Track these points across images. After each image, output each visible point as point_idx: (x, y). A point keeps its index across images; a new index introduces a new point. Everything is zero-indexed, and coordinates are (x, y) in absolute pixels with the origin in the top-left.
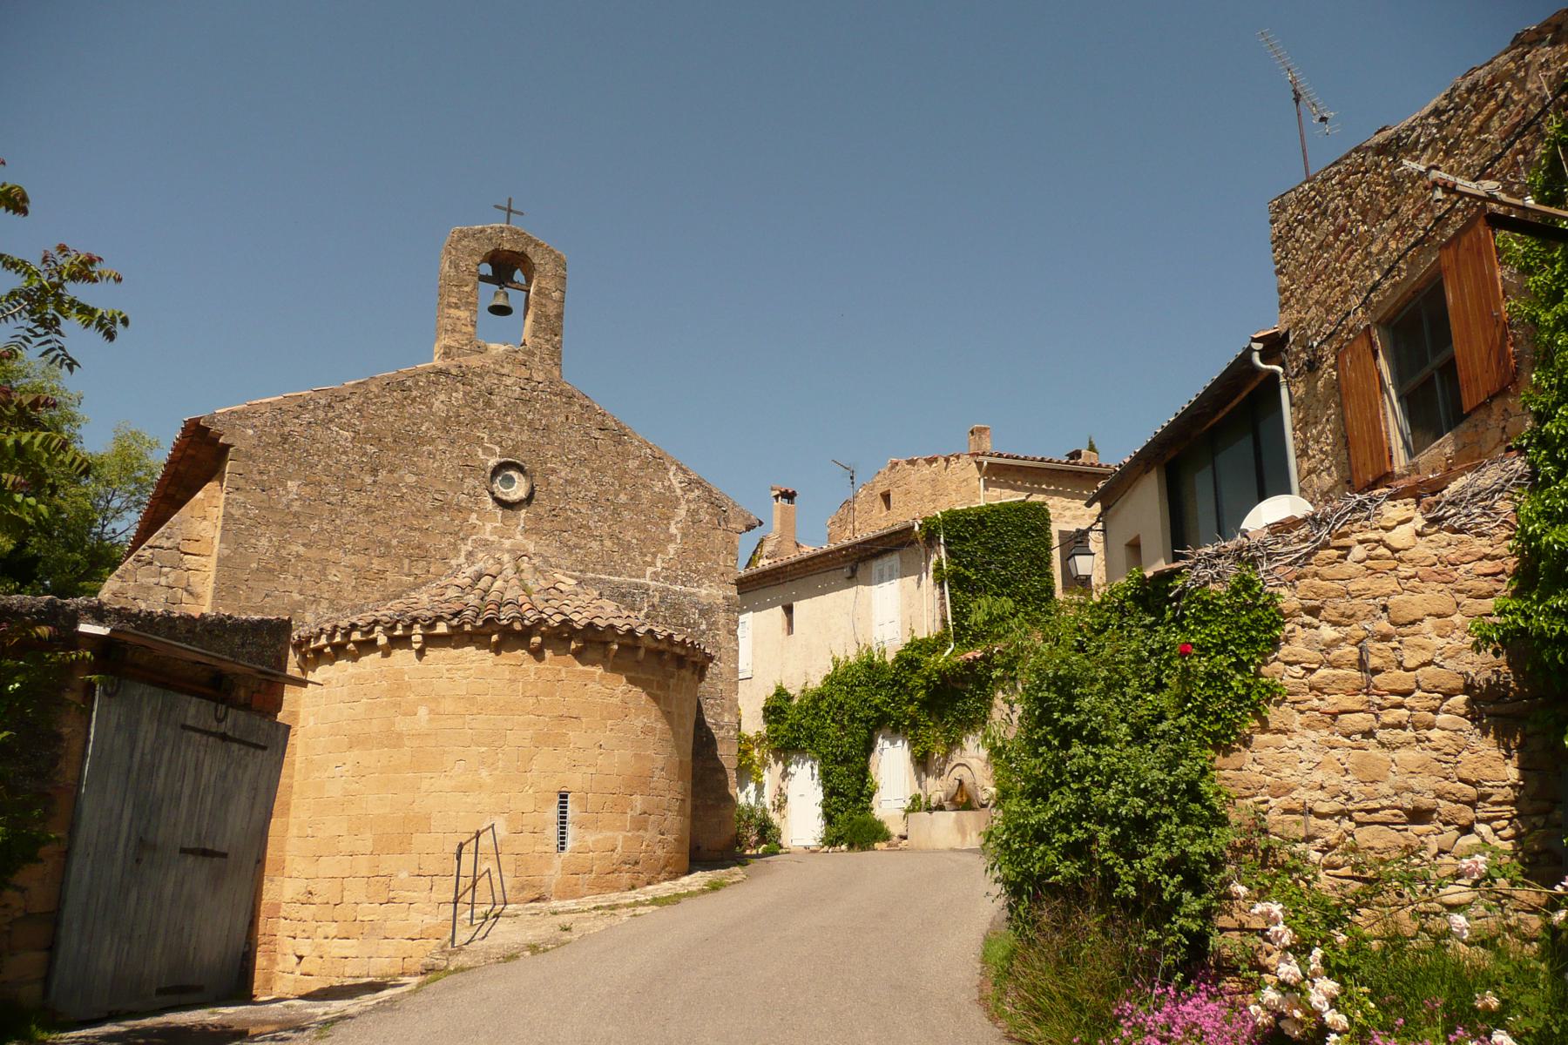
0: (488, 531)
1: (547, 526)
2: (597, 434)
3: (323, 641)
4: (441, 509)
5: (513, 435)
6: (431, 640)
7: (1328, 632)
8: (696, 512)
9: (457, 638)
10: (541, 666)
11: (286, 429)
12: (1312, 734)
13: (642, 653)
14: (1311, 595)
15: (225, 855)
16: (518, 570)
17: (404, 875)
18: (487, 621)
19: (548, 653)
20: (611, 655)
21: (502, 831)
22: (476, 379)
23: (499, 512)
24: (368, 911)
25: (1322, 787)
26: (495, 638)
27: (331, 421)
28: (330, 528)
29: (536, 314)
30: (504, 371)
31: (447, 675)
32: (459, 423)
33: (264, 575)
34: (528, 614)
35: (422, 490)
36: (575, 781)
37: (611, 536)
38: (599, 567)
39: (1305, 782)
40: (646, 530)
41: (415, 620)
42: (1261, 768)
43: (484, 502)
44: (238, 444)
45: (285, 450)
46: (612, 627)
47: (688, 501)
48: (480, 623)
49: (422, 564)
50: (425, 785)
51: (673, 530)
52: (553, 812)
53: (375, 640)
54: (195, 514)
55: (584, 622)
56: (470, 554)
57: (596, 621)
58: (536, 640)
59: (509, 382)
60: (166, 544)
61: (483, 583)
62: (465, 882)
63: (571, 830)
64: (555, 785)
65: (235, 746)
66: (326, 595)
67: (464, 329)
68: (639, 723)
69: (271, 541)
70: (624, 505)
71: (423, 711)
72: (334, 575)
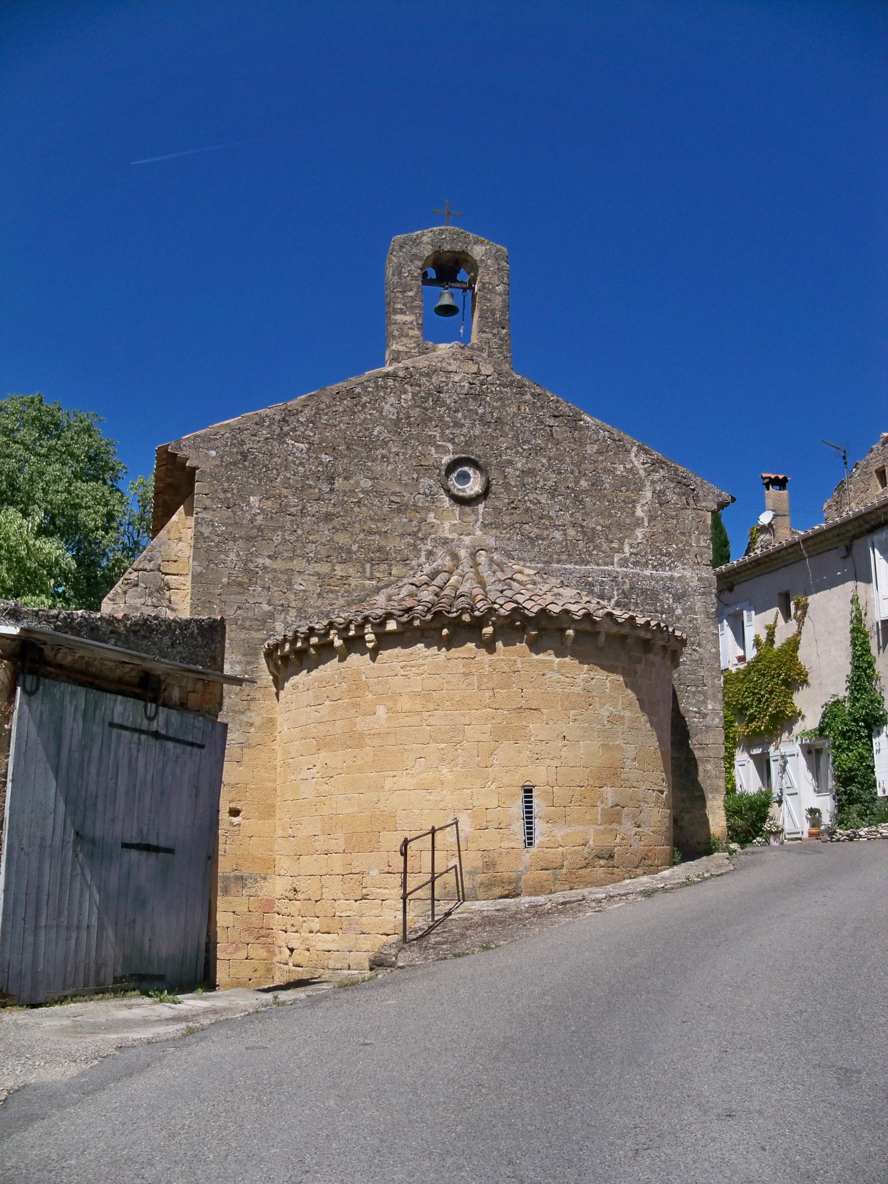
0: (446, 530)
1: (507, 520)
2: (551, 422)
3: (287, 647)
4: (399, 511)
5: (465, 430)
6: (386, 641)
8: (662, 493)
9: (407, 636)
10: (493, 657)
11: (245, 447)
13: (602, 638)
15: (170, 851)
16: (475, 565)
17: (374, 873)
18: (438, 614)
19: (499, 644)
20: (569, 643)
21: (466, 826)
22: (424, 380)
23: (457, 509)
24: (347, 908)
26: (445, 632)
27: (287, 435)
28: (293, 538)
29: (481, 310)
30: (450, 368)
32: (409, 424)
33: (236, 589)
34: (479, 605)
35: (380, 494)
36: (539, 775)
37: (574, 525)
38: (564, 557)
40: (610, 515)
43: (439, 500)
44: (203, 467)
45: (245, 468)
46: (567, 612)
48: (429, 617)
50: (389, 783)
51: (639, 513)
52: (517, 807)
53: (332, 642)
54: (172, 536)
55: (535, 610)
56: (430, 553)
58: (488, 630)
59: (457, 378)
60: (149, 566)
61: (439, 581)
63: (539, 825)
65: (170, 745)
67: (411, 333)
68: (604, 712)
69: (238, 555)
70: (585, 491)
71: (381, 710)
72: (300, 584)
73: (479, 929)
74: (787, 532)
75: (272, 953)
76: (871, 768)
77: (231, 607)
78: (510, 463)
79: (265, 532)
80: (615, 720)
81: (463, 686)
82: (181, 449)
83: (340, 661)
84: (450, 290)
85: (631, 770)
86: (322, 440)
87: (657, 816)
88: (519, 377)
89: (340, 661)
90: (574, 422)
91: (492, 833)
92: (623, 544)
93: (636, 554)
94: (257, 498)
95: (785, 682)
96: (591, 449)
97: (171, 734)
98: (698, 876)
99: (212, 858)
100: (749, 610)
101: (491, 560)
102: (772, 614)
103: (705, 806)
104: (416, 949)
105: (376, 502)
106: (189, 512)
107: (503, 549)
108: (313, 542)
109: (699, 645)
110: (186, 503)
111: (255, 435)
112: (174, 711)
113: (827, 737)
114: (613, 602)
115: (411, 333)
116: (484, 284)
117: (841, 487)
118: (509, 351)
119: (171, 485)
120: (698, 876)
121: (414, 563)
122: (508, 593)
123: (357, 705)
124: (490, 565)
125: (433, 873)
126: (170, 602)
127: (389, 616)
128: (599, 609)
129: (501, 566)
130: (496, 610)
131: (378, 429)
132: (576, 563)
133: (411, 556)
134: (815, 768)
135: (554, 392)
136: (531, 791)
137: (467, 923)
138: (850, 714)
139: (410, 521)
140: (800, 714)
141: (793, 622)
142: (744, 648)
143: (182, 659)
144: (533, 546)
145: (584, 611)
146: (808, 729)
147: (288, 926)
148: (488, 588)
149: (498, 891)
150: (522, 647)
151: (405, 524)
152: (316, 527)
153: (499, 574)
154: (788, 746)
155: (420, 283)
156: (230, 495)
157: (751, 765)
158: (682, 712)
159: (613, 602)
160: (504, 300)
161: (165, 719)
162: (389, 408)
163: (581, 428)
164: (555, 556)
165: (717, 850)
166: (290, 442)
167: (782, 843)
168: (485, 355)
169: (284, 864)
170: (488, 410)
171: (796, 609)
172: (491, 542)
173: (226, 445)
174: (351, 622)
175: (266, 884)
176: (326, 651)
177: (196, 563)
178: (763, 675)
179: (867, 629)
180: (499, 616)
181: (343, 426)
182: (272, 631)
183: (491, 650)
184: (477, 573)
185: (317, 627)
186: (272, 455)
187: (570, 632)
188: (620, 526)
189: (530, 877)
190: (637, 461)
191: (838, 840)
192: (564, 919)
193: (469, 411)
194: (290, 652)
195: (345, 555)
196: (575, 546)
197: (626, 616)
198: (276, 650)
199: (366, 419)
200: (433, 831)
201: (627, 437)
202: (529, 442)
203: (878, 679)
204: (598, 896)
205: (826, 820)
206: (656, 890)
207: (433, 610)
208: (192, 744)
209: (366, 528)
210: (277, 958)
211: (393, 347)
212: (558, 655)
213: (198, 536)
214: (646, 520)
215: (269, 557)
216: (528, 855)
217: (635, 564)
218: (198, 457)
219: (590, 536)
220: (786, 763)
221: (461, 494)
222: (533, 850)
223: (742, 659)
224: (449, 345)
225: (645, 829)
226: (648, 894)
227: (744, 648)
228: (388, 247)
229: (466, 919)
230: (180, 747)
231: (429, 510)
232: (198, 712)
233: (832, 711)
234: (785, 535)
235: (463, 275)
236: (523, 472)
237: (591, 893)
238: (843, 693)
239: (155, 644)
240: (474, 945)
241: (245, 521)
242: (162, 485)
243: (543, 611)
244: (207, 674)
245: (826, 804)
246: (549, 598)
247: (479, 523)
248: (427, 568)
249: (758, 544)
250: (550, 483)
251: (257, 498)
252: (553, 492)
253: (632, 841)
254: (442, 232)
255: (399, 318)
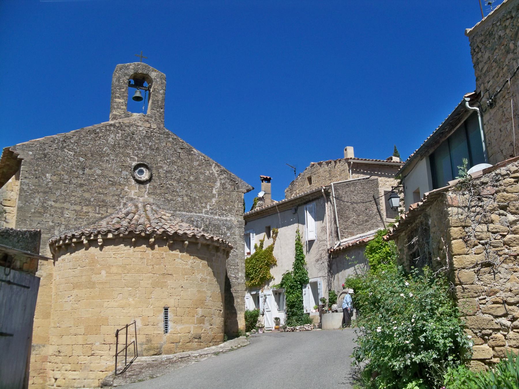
1: (158, 191)
2: (180, 151)
3: (61, 242)
4: (112, 185)
5: (143, 152)
6: (107, 242)
7: (511, 218)
9: (117, 241)
10: (154, 251)
11: (46, 152)
12: (505, 266)
13: (200, 245)
14: (502, 200)
15: (11, 335)
17: (97, 344)
18: (131, 232)
19: (156, 246)
20: (186, 247)
21: (139, 324)
22: (127, 128)
24: (84, 359)
25: (511, 291)
26: (133, 240)
27: (65, 147)
29: (153, 100)
30: (138, 124)
31: (113, 256)
32: (119, 147)
33: (37, 215)
34: (148, 229)
35: (104, 177)
36: (171, 303)
37: (187, 195)
38: (182, 209)
39: (502, 288)
40: (202, 192)
41: (99, 232)
42: (482, 283)
43: (130, 181)
44: (26, 159)
45: (45, 161)
46: (185, 234)
47: (221, 179)
48: (127, 233)
49: (105, 209)
50: (105, 304)
51: (214, 192)
52: (162, 316)
53: (83, 241)
55: (173, 232)
56: (125, 204)
57: (178, 231)
58: (152, 240)
61: (129, 217)
62: (121, 347)
63: (170, 324)
64: (162, 304)
65: (15, 287)
66: (63, 223)
67: (122, 107)
68: (199, 276)
70: (192, 181)
71: (103, 272)
73: (147, 369)
74: (270, 201)
75: (45, 381)
76: (302, 301)
77: (35, 222)
78: (161, 167)
79: (53, 190)
80: (203, 280)
81: (140, 263)
82: (16, 150)
83: (86, 250)
84: (140, 90)
85: (209, 302)
86: (80, 151)
87: (218, 321)
88: (167, 131)
89: (86, 250)
90: (189, 152)
91: (150, 327)
92: (207, 204)
93: (212, 209)
94: (50, 175)
95: (267, 264)
96: (196, 164)
97: (16, 282)
98: (236, 346)
99: (29, 338)
100: (253, 233)
101: (152, 209)
102: (263, 235)
103: (236, 317)
104: (121, 378)
105: (103, 180)
106: (17, 178)
107: (156, 204)
108: (74, 196)
109: (236, 249)
110: (17, 174)
111: (50, 146)
112: (17, 272)
113: (284, 288)
114: (202, 229)
115: (122, 107)
116: (155, 89)
117: (292, 183)
118: (163, 119)
119: (8, 165)
120: (236, 346)
121: (118, 208)
122: (160, 224)
123: (92, 270)
124: (152, 211)
125: (126, 344)
126: (6, 219)
127: (109, 231)
128: (199, 232)
129: (156, 212)
130: (156, 232)
131: (105, 148)
132: (187, 212)
133: (117, 205)
134: (278, 301)
135: (181, 138)
136: (167, 309)
137: (141, 366)
138: (294, 278)
139: (117, 189)
140: (273, 278)
141: (271, 240)
142: (250, 249)
143: (22, 248)
144: (169, 203)
145: (192, 234)
146: (276, 284)
147: (55, 368)
148: (151, 221)
149: (152, 352)
150: (166, 248)
151: (115, 191)
152: (75, 189)
153: (156, 215)
154: (267, 292)
155: (127, 86)
156: (37, 172)
157: (251, 299)
158: (228, 277)
159: (202, 229)
160: (163, 97)
161: (13, 276)
162: (111, 139)
163: (192, 154)
164: (178, 208)
165: (241, 335)
166: (66, 151)
167: (264, 332)
168: (153, 120)
169: (54, 339)
170: (153, 144)
171: (273, 234)
172: (151, 201)
173: (37, 150)
174: (92, 233)
175: (44, 349)
176: (79, 245)
177: (20, 202)
178: (258, 261)
179: (302, 244)
180: (157, 234)
181: (90, 146)
182: (53, 235)
183: (153, 248)
184: (146, 214)
185: (76, 234)
186: (58, 156)
187: (187, 242)
188: (206, 197)
189: (166, 346)
190: (215, 170)
191: (287, 331)
192: (183, 365)
193: (145, 143)
194: (62, 245)
195: (88, 203)
196: (187, 204)
197: (210, 237)
198: (56, 243)
199: (100, 143)
200: (127, 326)
201: (211, 159)
202: (170, 159)
203: (306, 264)
204: (195, 355)
205: (282, 322)
206: (219, 353)
207: (128, 230)
208: (25, 287)
209: (98, 191)
210: (48, 383)
211: (114, 113)
212: (181, 252)
213: (21, 190)
214: (217, 195)
215: (54, 201)
216: (165, 337)
217: (212, 213)
218: (23, 154)
219: (193, 200)
220: (266, 298)
221: (140, 179)
222: (168, 334)
223: (249, 253)
224: (138, 114)
225: (214, 326)
226: (217, 354)
227: (250, 249)
228: (115, 68)
229: (140, 365)
230: (19, 288)
231: (125, 185)
232: (27, 272)
233: (286, 277)
234: (269, 203)
235: (146, 84)
236: (167, 171)
237: (192, 353)
238: (291, 269)
239: (10, 241)
240: (146, 376)
241: (43, 185)
242: (3, 165)
243: (176, 233)
244: (33, 255)
245: (282, 316)
246: (177, 227)
247: (147, 192)
248: (124, 211)
249: (257, 205)
250: (178, 177)
251: (50, 175)
252: (179, 181)
253: (209, 331)
254: (138, 65)
255: (117, 100)
